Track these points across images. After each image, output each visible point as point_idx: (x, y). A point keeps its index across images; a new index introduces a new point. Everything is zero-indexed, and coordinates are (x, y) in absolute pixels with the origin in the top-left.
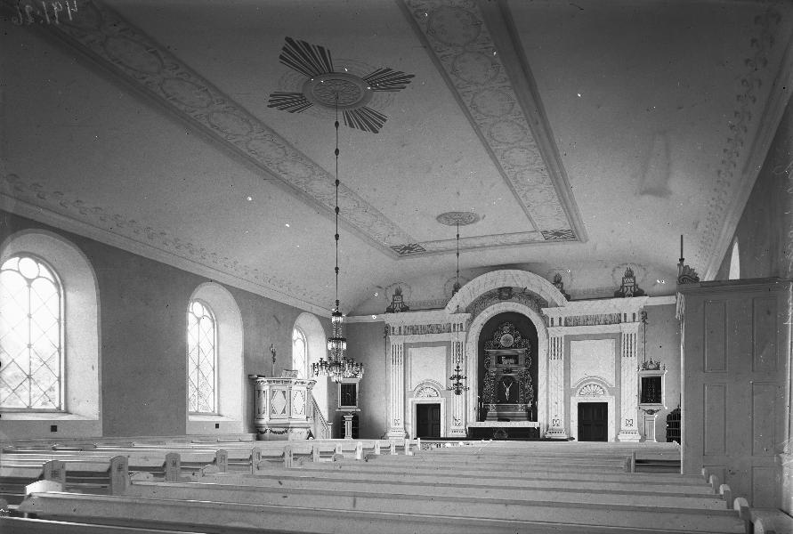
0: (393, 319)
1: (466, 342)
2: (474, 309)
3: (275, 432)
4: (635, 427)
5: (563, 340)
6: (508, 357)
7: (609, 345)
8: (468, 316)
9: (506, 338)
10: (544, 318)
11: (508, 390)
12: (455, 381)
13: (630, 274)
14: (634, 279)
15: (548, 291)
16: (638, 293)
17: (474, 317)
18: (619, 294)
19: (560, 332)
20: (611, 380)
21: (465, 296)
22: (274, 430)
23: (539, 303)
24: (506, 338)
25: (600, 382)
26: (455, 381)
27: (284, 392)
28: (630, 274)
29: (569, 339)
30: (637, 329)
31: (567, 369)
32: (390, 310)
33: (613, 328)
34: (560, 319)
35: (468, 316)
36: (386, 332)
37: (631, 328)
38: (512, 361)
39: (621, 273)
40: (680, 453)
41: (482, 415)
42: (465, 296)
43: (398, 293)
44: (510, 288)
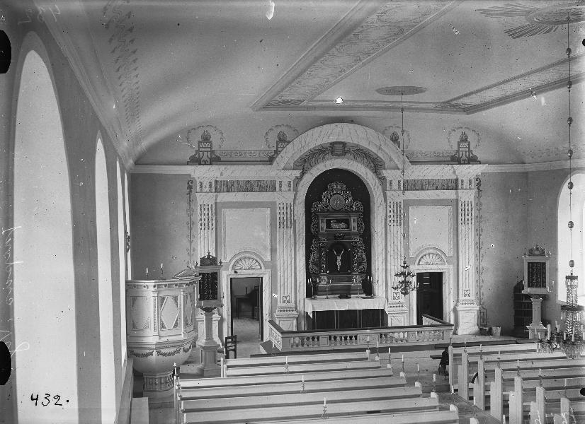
0: (203, 174)
1: (294, 203)
2: (304, 163)
3: (164, 355)
4: (473, 297)
5: (402, 206)
6: (338, 221)
7: (446, 211)
8: (298, 173)
9: (337, 198)
10: (382, 180)
11: (339, 258)
12: (402, 279)
13: (464, 139)
14: (469, 145)
15: (387, 152)
16: (472, 160)
17: (303, 174)
18: (456, 160)
19: (396, 196)
20: (447, 248)
21: (291, 153)
22: (163, 351)
23: (376, 165)
24: (337, 198)
25: (439, 253)
26: (402, 279)
27: (176, 299)
28: (464, 139)
29: (408, 204)
30: (473, 196)
31: (406, 236)
32: (195, 161)
33: (450, 194)
34: (399, 182)
35: (298, 173)
36: (190, 188)
37: (467, 196)
38: (342, 225)
39: (456, 137)
40: (345, 294)
41: (312, 292)
42: (291, 153)
43: (206, 139)
44: (344, 144)
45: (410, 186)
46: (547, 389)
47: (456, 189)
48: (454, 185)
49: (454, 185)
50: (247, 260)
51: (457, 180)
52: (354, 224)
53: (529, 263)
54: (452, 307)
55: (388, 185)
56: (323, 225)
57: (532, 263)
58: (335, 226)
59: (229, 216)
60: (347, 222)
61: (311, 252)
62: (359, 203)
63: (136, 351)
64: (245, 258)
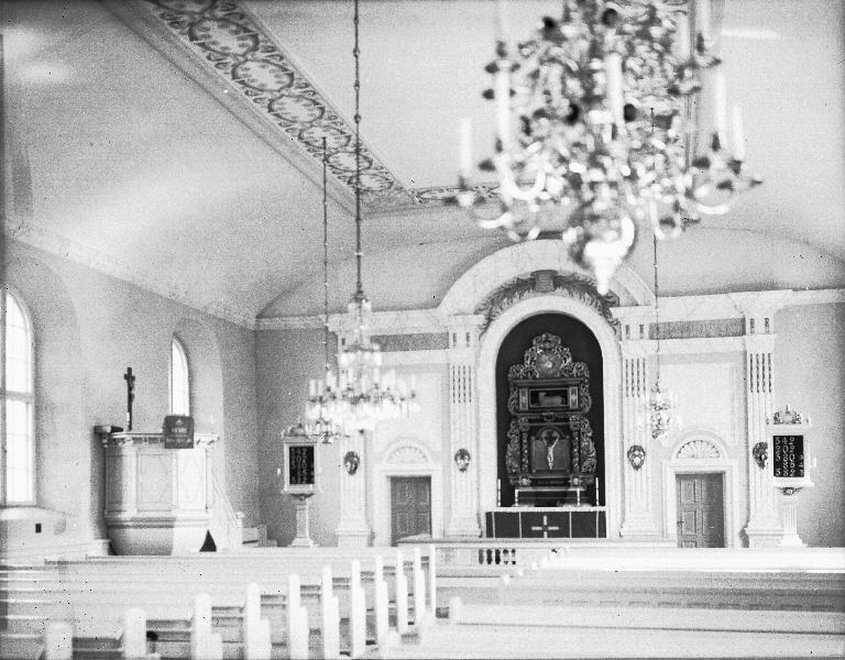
10: (614, 324)
33: (734, 343)
38: (558, 400)
45: (658, 332)
46: (385, 558)
47: (744, 333)
48: (740, 328)
49: (740, 328)
50: (421, 456)
51: (743, 320)
52: (573, 398)
53: (290, 448)
54: (738, 529)
55: (624, 332)
56: (524, 399)
57: (296, 448)
58: (546, 401)
59: (668, 373)
60: (565, 396)
61: (508, 441)
62: (582, 366)
63: (110, 524)
64: (421, 452)
